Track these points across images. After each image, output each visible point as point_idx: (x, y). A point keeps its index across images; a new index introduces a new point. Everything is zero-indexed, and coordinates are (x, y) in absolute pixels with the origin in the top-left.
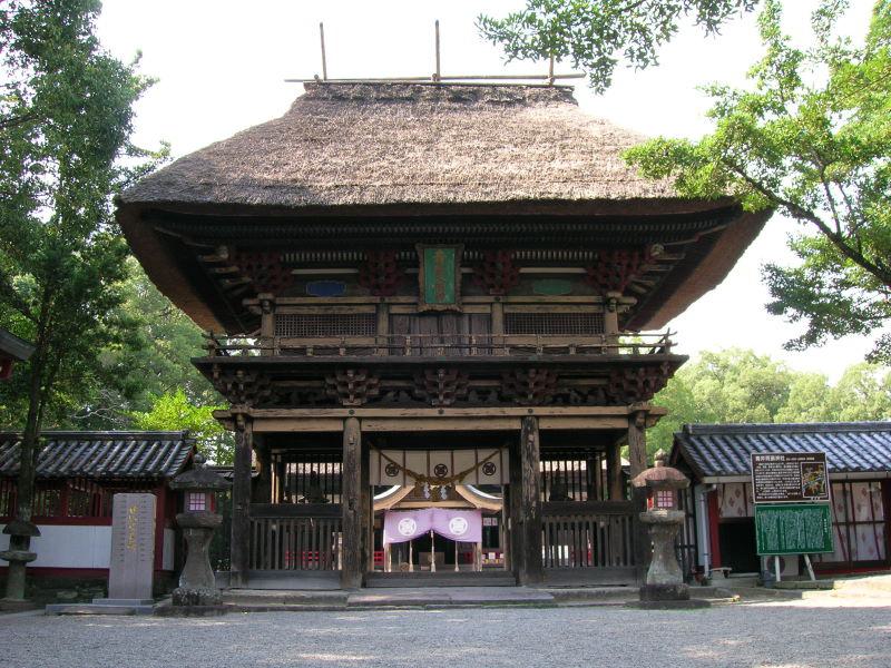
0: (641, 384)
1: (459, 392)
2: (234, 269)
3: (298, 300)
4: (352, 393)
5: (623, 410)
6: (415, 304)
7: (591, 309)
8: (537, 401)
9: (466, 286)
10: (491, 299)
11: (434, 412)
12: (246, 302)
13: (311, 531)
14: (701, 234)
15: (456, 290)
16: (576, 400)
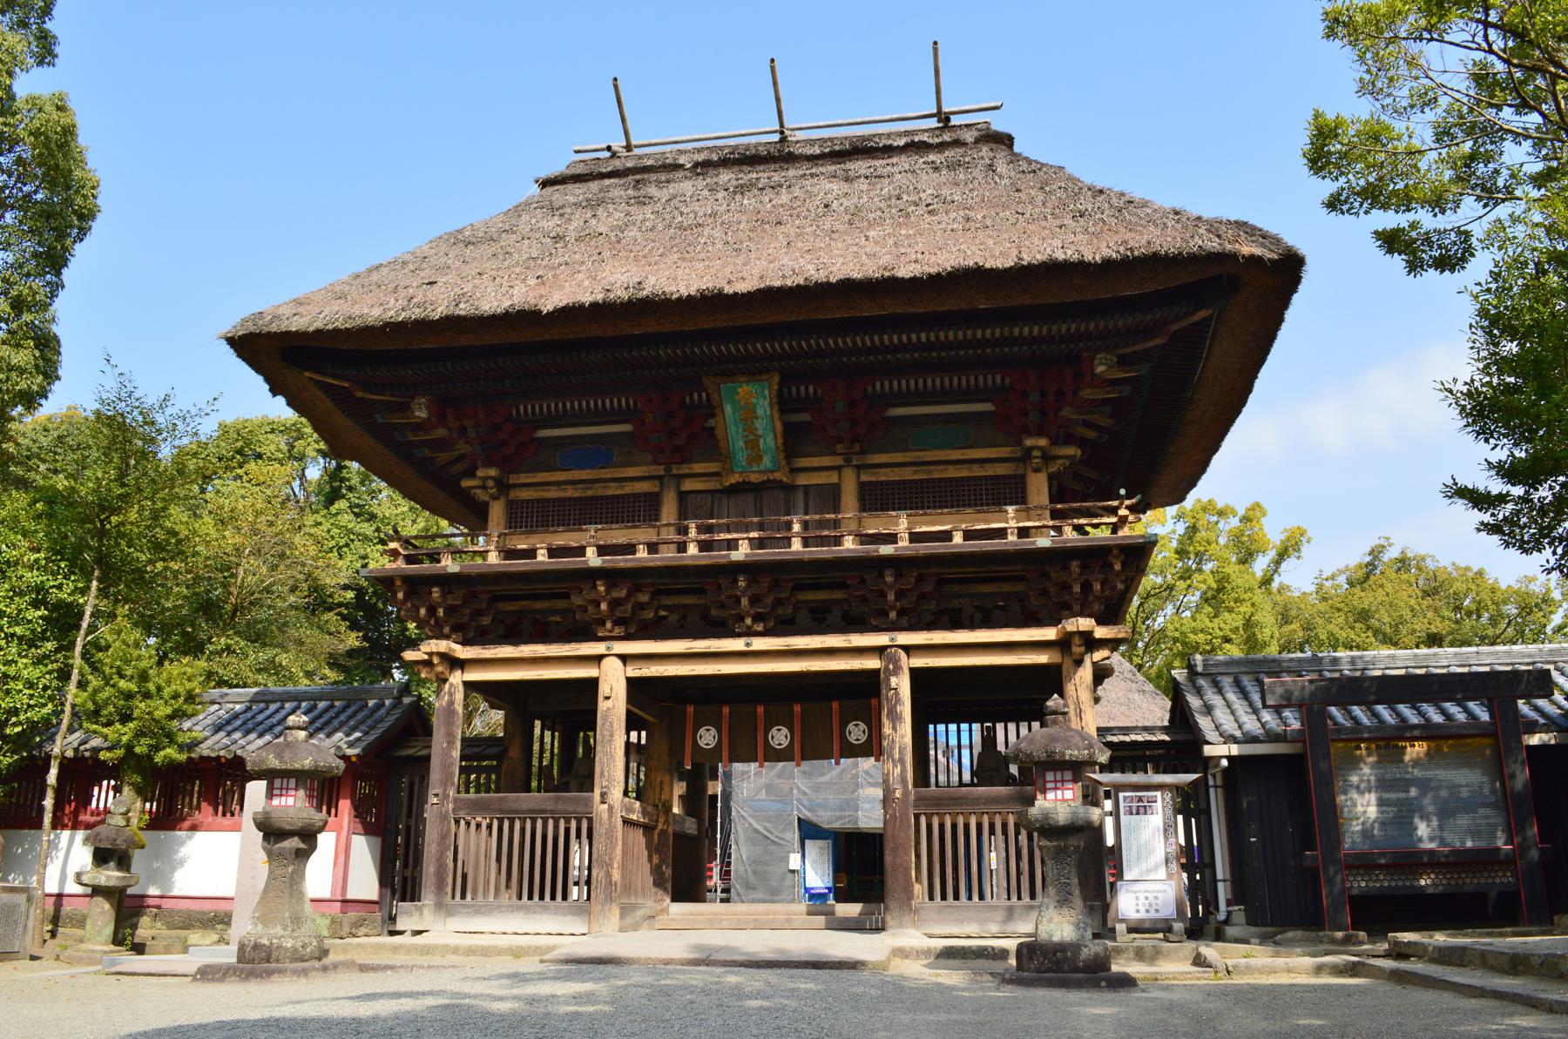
0: (1077, 589)
1: (780, 611)
2: (440, 433)
3: (542, 477)
4: (609, 617)
5: (1050, 634)
6: (717, 474)
7: (1001, 470)
8: (904, 621)
9: (794, 442)
10: (838, 461)
11: (737, 644)
12: (466, 483)
13: (578, 836)
14: (1176, 327)
15: (777, 448)
16: (972, 617)
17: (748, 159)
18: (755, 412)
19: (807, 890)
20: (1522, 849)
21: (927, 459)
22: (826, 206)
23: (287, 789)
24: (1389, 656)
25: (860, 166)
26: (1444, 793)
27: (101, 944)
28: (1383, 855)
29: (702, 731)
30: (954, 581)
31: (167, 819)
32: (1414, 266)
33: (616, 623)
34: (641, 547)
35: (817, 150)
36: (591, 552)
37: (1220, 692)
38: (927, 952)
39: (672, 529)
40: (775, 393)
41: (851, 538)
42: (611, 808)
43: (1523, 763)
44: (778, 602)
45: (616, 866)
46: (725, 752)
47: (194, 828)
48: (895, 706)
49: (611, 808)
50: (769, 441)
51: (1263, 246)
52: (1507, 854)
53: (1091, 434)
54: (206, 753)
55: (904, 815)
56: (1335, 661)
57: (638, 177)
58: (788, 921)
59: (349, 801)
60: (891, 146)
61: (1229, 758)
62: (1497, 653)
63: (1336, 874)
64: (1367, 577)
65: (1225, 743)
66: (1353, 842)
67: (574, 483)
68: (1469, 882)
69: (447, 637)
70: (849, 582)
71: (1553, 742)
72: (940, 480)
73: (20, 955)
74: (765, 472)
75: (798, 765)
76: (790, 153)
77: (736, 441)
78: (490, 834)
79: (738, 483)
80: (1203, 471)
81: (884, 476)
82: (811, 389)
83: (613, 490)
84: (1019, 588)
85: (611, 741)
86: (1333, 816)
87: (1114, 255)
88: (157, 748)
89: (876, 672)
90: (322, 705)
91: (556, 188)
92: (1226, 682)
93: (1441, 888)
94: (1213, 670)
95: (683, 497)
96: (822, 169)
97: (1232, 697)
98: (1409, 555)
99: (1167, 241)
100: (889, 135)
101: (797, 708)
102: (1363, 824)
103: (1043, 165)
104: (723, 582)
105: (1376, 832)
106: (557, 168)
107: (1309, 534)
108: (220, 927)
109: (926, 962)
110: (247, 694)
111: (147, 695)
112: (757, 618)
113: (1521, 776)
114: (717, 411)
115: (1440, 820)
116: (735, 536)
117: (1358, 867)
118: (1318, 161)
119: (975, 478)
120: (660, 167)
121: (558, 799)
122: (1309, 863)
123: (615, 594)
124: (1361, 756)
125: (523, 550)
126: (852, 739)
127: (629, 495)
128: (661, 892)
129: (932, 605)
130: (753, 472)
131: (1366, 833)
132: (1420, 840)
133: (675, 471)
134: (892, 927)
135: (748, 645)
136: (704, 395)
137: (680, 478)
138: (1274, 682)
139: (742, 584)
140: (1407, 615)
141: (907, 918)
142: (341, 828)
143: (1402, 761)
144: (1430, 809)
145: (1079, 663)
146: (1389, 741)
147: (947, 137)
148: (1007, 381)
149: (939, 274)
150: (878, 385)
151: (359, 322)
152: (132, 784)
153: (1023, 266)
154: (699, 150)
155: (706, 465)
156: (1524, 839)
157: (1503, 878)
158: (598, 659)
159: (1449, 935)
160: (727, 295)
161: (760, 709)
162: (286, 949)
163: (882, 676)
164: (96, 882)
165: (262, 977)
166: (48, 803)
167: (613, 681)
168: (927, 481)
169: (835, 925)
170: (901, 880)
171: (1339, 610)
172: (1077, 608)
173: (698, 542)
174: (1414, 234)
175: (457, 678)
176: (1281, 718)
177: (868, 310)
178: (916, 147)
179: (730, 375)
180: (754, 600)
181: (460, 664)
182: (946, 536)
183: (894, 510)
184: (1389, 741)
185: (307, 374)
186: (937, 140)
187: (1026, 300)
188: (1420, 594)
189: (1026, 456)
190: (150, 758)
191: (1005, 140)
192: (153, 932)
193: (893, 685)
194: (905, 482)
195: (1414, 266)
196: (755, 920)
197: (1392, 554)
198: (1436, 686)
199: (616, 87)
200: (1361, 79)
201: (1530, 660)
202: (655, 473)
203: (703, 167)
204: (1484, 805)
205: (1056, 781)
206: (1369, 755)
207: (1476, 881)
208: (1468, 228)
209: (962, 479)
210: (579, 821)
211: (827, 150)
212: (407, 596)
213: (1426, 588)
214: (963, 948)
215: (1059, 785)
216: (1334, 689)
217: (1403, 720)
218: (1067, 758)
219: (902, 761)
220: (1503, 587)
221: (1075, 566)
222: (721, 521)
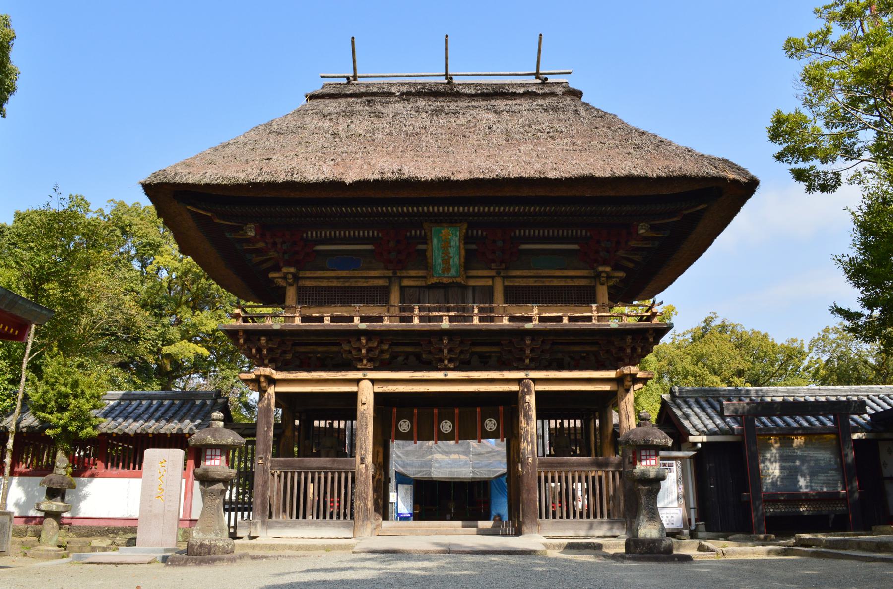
0: (629, 351)
2: (261, 245)
3: (319, 273)
4: (365, 357)
5: (612, 374)
6: (424, 277)
7: (583, 282)
8: (533, 365)
9: (470, 260)
10: (493, 273)
11: (439, 375)
12: (272, 275)
15: (460, 264)
18: (450, 243)
19: (398, 514)
20: (851, 493)
22: (490, 128)
23: (215, 455)
24: (774, 390)
25: (500, 103)
26: (812, 463)
27: (51, 546)
28: (782, 495)
29: (401, 422)
30: (562, 344)
31: (80, 469)
32: (810, 189)
33: (369, 360)
34: (386, 318)
36: (356, 320)
37: (690, 407)
38: (559, 546)
39: (397, 309)
40: (463, 234)
41: (507, 318)
42: (366, 466)
43: (852, 449)
44: (462, 352)
45: (369, 499)
46: (415, 434)
47: (93, 476)
48: (528, 411)
49: (366, 466)
50: (456, 260)
51: (739, 174)
52: (843, 495)
53: (631, 265)
54: (104, 430)
55: (533, 472)
56: (748, 391)
57: (369, 98)
58: (455, 530)
59: (193, 461)
60: (515, 93)
61: (702, 443)
62: (829, 389)
63: (759, 505)
64: (703, 336)
65: (700, 435)
66: (767, 488)
67: (338, 278)
68: (824, 509)
69: (266, 366)
70: (502, 342)
71: (864, 438)
72: (548, 286)
73: (5, 554)
74: (451, 277)
75: (415, 443)
76: (458, 92)
77: (437, 259)
78: (280, 481)
79: (436, 283)
80: (671, 283)
82: (480, 232)
83: (361, 283)
84: (595, 348)
85: (366, 428)
86: (757, 476)
87: (663, 174)
88: (82, 428)
89: (517, 393)
90: (166, 402)
91: (319, 100)
92: (691, 401)
93: (811, 512)
94: (684, 395)
95: (402, 289)
96: (477, 104)
97: (697, 410)
98: (727, 324)
99: (690, 169)
100: (513, 85)
101: (457, 410)
102: (772, 479)
103: (606, 113)
105: (779, 483)
107: (676, 310)
108: (111, 536)
109: (560, 551)
110: (118, 395)
111: (76, 396)
112: (450, 361)
113: (851, 456)
114: (429, 242)
115: (810, 477)
116: (441, 314)
117: (769, 501)
118: (775, 135)
119: (568, 286)
120: (381, 93)
121: (334, 461)
122: (745, 499)
123: (370, 345)
124: (772, 443)
125: (316, 317)
126: (488, 429)
127: (371, 287)
128: (377, 515)
129: (547, 357)
130: (445, 277)
131: (774, 484)
132: (801, 487)
133: (399, 274)
134: (527, 533)
135: (445, 375)
136: (423, 232)
137: (401, 278)
138: (729, 404)
139: (446, 341)
140: (727, 359)
141: (535, 528)
142: (189, 477)
143: (792, 446)
144: (806, 471)
145: (627, 391)
146: (786, 436)
147: (547, 90)
148: (589, 234)
149: (570, 178)
150: (413, 232)
151: (232, 181)
152: (64, 449)
153: (616, 177)
154: (402, 84)
155: (416, 271)
156: (852, 488)
157: (840, 508)
158: (357, 381)
159: (824, 536)
160: (453, 181)
161: (436, 411)
162: (219, 547)
163: (520, 394)
164: (50, 509)
165: (209, 563)
166: (8, 460)
167: (366, 394)
168: (542, 286)
169: (482, 533)
170: (532, 507)
171: (688, 354)
172: (627, 361)
173: (420, 316)
174: (811, 172)
175: (272, 390)
176: (725, 422)
177: (526, 192)
180: (451, 350)
181: (272, 381)
182: (559, 319)
184: (786, 436)
185: (188, 207)
186: (541, 92)
187: (612, 194)
188: (734, 347)
189: (598, 275)
190: (76, 434)
191: (577, 94)
192: (67, 539)
193: (527, 400)
194: (529, 287)
195: (810, 189)
196: (437, 530)
197: (717, 322)
198: (810, 408)
199: (353, 43)
200: (806, 98)
201: (845, 394)
202: (387, 275)
203: (406, 96)
204: (831, 470)
205: (646, 455)
206: (776, 443)
207: (827, 509)
208: (840, 172)
209: (561, 286)
210: (346, 473)
211: (479, 92)
213: (737, 343)
214: (578, 544)
215: (648, 457)
216: (759, 408)
217: (788, 424)
218: (655, 443)
219: (532, 442)
220: (779, 344)
222: (433, 305)
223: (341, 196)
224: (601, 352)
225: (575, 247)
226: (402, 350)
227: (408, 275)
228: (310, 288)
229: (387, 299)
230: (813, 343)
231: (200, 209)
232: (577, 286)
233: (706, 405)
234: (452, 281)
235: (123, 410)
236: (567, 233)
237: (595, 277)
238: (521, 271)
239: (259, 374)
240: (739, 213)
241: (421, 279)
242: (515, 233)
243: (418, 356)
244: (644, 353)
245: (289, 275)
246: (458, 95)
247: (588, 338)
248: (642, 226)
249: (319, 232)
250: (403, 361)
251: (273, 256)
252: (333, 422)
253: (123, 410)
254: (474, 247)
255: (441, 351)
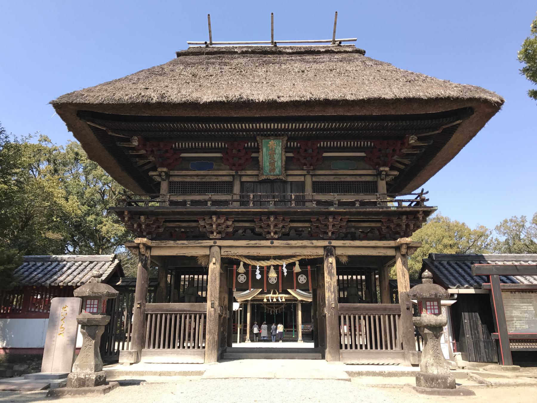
2: (143, 152)
5: (392, 243)
6: (257, 175)
7: (368, 179)
9: (288, 163)
10: (305, 172)
12: (151, 173)
14: (444, 127)
15: (282, 166)
17: (264, 52)
18: (275, 151)
21: (340, 173)
25: (308, 57)
33: (219, 233)
35: (290, 51)
48: (331, 270)
50: (279, 163)
53: (402, 167)
67: (197, 176)
70: (312, 220)
72: (344, 182)
81: (322, 179)
83: (214, 179)
84: (378, 225)
95: (242, 183)
98: (439, 217)
104: (263, 218)
106: (184, 48)
108: (28, 362)
112: (275, 233)
114: (260, 150)
119: (357, 182)
123: (219, 221)
127: (220, 182)
130: (271, 175)
133: (239, 173)
136: (256, 144)
137: (241, 176)
148: (299, 145)
150: (249, 144)
154: (243, 47)
178: (328, 52)
179: (267, 136)
183: (333, 192)
185: (88, 123)
187: (393, 113)
189: (379, 173)
191: (362, 52)
194: (330, 182)
202: (231, 174)
203: (244, 53)
209: (353, 182)
212: (129, 219)
221: (404, 217)
223: (198, 115)
224: (383, 227)
225: (363, 154)
226: (241, 225)
227: (246, 174)
228: (177, 183)
229: (231, 190)
230: (498, 228)
231: (96, 124)
232: (364, 182)
233: (463, 265)
234: (276, 178)
235: (44, 269)
236: (357, 144)
237: (376, 175)
238: (324, 171)
239: (139, 242)
240: (483, 128)
241: (255, 177)
242: (320, 144)
243: (253, 230)
244: (415, 228)
245: (163, 173)
246: (280, 53)
247: (373, 217)
248: (412, 138)
249: (184, 144)
250: (242, 233)
251: (151, 160)
252: (194, 276)
253: (44, 269)
254: (291, 155)
255: (269, 226)
